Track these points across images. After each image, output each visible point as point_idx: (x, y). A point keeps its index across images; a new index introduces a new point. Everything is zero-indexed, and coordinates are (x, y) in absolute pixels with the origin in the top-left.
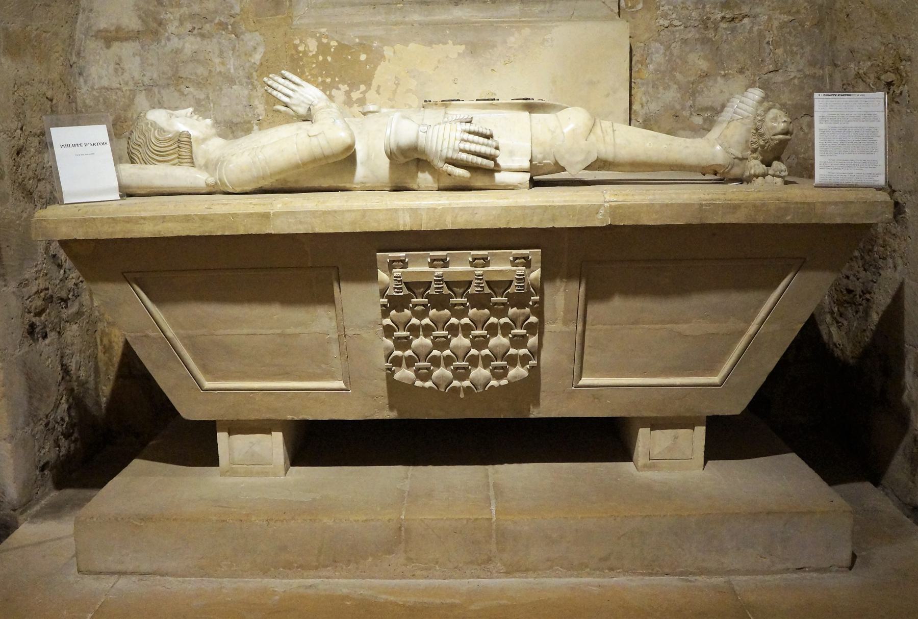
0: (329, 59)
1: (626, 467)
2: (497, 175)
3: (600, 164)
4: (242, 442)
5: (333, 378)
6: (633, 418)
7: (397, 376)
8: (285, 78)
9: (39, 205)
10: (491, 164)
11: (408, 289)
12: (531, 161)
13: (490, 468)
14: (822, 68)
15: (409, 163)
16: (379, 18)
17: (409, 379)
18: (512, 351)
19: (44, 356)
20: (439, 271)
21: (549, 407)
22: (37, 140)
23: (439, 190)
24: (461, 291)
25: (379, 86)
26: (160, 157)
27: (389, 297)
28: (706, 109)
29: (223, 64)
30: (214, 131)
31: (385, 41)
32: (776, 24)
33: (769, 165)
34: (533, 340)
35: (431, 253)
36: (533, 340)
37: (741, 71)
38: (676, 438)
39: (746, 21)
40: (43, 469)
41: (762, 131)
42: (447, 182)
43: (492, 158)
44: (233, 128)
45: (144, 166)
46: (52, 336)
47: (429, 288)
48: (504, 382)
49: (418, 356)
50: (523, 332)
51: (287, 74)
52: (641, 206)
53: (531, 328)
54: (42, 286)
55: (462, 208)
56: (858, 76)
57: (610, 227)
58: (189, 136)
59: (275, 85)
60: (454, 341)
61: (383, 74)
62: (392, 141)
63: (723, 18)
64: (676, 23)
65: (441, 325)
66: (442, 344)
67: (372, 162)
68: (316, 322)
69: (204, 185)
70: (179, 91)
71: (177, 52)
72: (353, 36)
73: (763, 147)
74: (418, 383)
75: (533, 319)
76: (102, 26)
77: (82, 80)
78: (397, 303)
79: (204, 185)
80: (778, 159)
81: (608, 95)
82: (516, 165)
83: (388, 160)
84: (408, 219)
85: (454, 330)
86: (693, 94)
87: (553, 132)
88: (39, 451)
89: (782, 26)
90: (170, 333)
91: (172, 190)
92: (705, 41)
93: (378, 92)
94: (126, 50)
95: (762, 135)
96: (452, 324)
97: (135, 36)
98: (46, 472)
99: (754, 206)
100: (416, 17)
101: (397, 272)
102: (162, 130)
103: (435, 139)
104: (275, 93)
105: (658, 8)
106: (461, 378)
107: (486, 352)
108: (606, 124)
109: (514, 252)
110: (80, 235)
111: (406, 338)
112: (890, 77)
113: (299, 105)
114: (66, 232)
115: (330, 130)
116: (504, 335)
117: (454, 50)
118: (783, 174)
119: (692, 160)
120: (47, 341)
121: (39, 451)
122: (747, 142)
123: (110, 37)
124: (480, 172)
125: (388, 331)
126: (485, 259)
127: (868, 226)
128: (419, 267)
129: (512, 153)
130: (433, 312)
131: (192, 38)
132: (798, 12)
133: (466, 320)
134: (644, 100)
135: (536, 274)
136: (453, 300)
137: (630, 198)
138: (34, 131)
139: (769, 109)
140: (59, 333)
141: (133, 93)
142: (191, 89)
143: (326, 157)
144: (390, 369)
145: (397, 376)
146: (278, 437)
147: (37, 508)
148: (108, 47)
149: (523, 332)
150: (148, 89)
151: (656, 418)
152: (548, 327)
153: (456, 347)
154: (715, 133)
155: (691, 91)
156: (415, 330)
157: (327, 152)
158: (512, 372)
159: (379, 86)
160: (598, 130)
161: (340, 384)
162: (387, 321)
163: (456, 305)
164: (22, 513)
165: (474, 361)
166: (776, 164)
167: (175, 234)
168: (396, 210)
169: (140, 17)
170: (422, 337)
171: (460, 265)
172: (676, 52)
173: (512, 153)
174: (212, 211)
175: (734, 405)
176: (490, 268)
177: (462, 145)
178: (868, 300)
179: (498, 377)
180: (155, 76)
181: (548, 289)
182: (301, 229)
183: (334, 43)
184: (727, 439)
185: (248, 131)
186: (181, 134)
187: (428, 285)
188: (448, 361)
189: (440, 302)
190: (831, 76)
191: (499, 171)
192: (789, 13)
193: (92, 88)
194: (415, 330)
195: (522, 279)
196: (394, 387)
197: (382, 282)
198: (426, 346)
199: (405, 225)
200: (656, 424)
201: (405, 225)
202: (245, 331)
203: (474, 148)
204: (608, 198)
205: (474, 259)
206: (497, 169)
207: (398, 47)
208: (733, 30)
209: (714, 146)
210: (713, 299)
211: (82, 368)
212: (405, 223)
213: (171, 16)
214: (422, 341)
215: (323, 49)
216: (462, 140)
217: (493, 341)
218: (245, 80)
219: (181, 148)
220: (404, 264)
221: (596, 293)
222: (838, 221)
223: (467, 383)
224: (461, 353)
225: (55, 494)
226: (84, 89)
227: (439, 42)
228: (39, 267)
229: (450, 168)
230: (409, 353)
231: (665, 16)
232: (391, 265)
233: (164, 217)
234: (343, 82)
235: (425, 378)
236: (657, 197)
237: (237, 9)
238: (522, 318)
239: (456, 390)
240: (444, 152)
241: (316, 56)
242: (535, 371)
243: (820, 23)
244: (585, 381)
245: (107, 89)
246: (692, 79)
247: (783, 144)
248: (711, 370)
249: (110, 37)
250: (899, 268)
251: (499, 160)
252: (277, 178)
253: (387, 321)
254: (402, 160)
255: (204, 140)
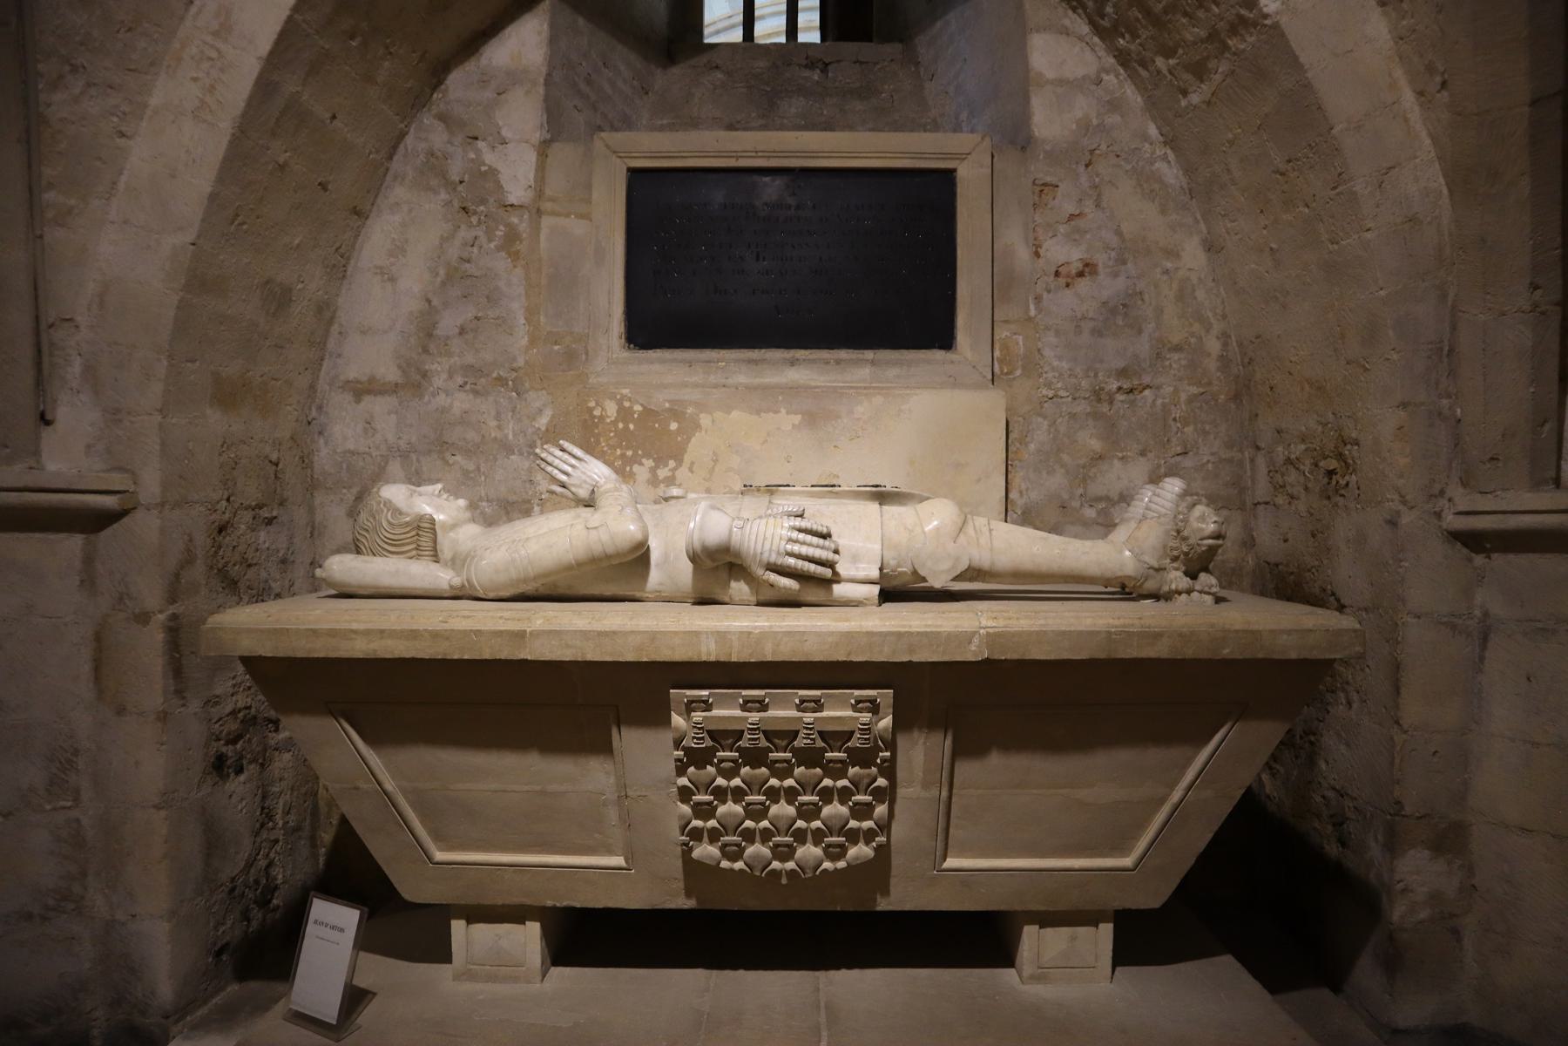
0: (631, 426)
1: (1008, 975)
2: (836, 587)
3: (973, 573)
4: (484, 932)
5: (610, 852)
6: (1015, 912)
7: (696, 854)
8: (563, 450)
9: (246, 598)
10: (828, 572)
11: (712, 739)
12: (881, 569)
13: (821, 975)
14: (1241, 451)
15: (719, 568)
16: (694, 379)
17: (711, 857)
18: (853, 824)
19: (235, 799)
20: (754, 717)
21: (902, 896)
22: (250, 514)
23: (759, 604)
24: (784, 743)
25: (693, 463)
26: (393, 547)
27: (684, 749)
28: (1099, 499)
29: (499, 427)
30: (468, 515)
31: (701, 407)
32: (1183, 397)
33: (1194, 577)
34: (881, 810)
35: (745, 692)
36: (881, 810)
37: (1143, 453)
38: (1073, 938)
39: (1147, 392)
40: (219, 953)
41: (1185, 533)
42: (768, 595)
43: (831, 565)
44: (511, 507)
45: (370, 558)
46: (252, 770)
47: (740, 738)
48: (841, 864)
49: (725, 828)
50: (868, 798)
51: (566, 445)
52: (1030, 633)
53: (879, 795)
54: (240, 704)
55: (789, 633)
56: (1289, 461)
57: (987, 661)
58: (432, 522)
59: (550, 458)
60: (774, 810)
61: (697, 448)
62: (696, 537)
63: (1120, 388)
64: (1062, 393)
65: (756, 788)
66: (758, 813)
67: (670, 565)
68: (590, 777)
69: (446, 587)
70: (443, 459)
71: (444, 411)
72: (661, 400)
73: (1186, 554)
74: (725, 864)
75: (881, 782)
76: (352, 375)
77: (322, 441)
78: (697, 758)
79: (446, 587)
80: (1206, 570)
81: (979, 480)
82: (861, 574)
83: (689, 566)
84: (713, 646)
85: (773, 795)
86: (1084, 480)
87: (911, 531)
88: (216, 928)
89: (1190, 401)
90: (389, 785)
91: (404, 592)
92: (1095, 416)
93: (691, 470)
94: (379, 406)
95: (1185, 539)
96: (772, 787)
97: (394, 389)
98: (224, 957)
99: (1181, 635)
100: (742, 379)
101: (698, 716)
102: (398, 512)
103: (753, 538)
104: (549, 469)
105: (1040, 376)
106: (784, 858)
107: (817, 824)
108: (981, 521)
109: (857, 692)
110: (266, 650)
111: (709, 803)
112: (1333, 464)
113: (579, 486)
114: (249, 646)
115: (616, 522)
116: (842, 803)
117: (787, 420)
118: (1214, 590)
119: (1094, 570)
120: (242, 778)
121: (216, 928)
122: (1165, 547)
123: (362, 390)
124: (813, 583)
125: (685, 795)
126: (817, 701)
127: (1329, 663)
128: (727, 711)
129: (855, 558)
130: (745, 770)
131: (461, 395)
132: (1210, 384)
133: (790, 782)
134: (1023, 487)
135: (886, 722)
136: (774, 755)
137: (1014, 622)
138: (246, 503)
139: (1194, 505)
140: (262, 765)
141: (386, 459)
142: (458, 458)
143: (608, 557)
144: (686, 844)
145: (696, 854)
146: (534, 928)
147: (202, 1012)
148: (358, 401)
149: (868, 798)
150: (404, 456)
151: (1047, 913)
152: (901, 792)
153: (776, 817)
154: (1120, 534)
155: (1082, 477)
156: (721, 794)
157: (610, 550)
158: (853, 852)
159: (693, 463)
160: (970, 529)
161: (618, 861)
162: (683, 781)
163: (777, 761)
164: (177, 1021)
165: (800, 837)
166: (1203, 576)
167: (397, 655)
168: (697, 634)
169: (399, 367)
170: (730, 803)
171: (783, 710)
172: (1062, 429)
173: (855, 558)
174: (447, 626)
175: (1152, 897)
176: (825, 714)
177: (789, 547)
178: (1312, 743)
179: (834, 858)
180: (414, 439)
181: (902, 742)
182: (567, 655)
183: (638, 408)
184: (1142, 939)
185: (527, 513)
186: (421, 518)
187: (739, 735)
188: (766, 835)
189: (755, 757)
190: (1252, 461)
191: (838, 582)
192: (1199, 384)
193: (335, 452)
194: (721, 794)
195: (867, 729)
196: (692, 868)
197: (677, 729)
198: (736, 815)
199: (709, 654)
200: (1047, 920)
201: (709, 654)
202: (493, 786)
203: (804, 550)
204: (984, 623)
205: (802, 702)
206: (836, 578)
207: (718, 415)
208: (1132, 403)
209: (1121, 552)
210: (1124, 756)
211: (293, 811)
212: (709, 651)
213: (438, 367)
214: (730, 808)
215: (625, 414)
216: (790, 540)
217: (827, 811)
218: (525, 450)
219: (422, 537)
220: (708, 706)
221: (968, 747)
222: (1293, 655)
223: (791, 865)
224: (783, 825)
225: (234, 988)
226: (324, 452)
227: (768, 410)
228: (239, 679)
229: (773, 577)
230: (712, 823)
231: (1049, 385)
232: (690, 706)
233: (382, 631)
234: (648, 455)
235: (734, 858)
236: (1050, 622)
237: (521, 362)
238: (866, 781)
239: (776, 874)
240: (766, 555)
241: (615, 423)
242: (883, 852)
243: (1236, 397)
244: (951, 862)
245: (353, 453)
246: (1082, 462)
247: (1212, 550)
248: (1119, 849)
249: (362, 390)
250: (1355, 706)
251: (839, 568)
252: (544, 581)
253: (683, 781)
254: (709, 564)
255: (454, 526)
